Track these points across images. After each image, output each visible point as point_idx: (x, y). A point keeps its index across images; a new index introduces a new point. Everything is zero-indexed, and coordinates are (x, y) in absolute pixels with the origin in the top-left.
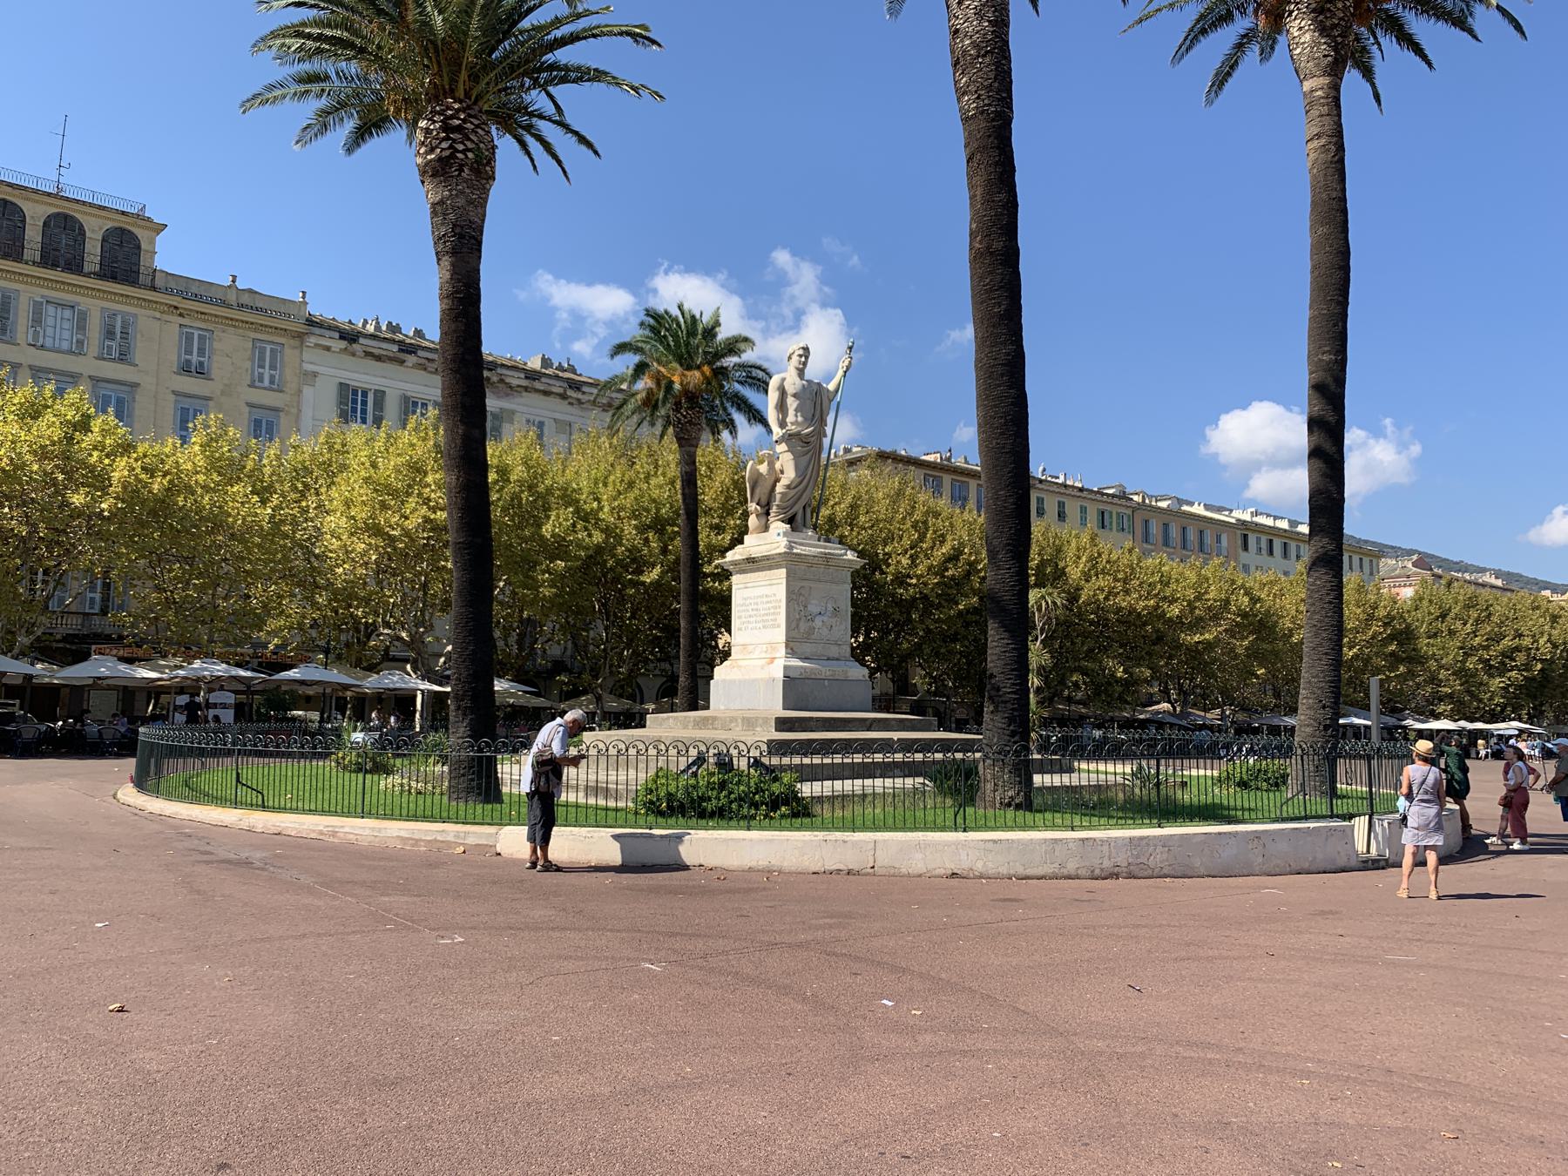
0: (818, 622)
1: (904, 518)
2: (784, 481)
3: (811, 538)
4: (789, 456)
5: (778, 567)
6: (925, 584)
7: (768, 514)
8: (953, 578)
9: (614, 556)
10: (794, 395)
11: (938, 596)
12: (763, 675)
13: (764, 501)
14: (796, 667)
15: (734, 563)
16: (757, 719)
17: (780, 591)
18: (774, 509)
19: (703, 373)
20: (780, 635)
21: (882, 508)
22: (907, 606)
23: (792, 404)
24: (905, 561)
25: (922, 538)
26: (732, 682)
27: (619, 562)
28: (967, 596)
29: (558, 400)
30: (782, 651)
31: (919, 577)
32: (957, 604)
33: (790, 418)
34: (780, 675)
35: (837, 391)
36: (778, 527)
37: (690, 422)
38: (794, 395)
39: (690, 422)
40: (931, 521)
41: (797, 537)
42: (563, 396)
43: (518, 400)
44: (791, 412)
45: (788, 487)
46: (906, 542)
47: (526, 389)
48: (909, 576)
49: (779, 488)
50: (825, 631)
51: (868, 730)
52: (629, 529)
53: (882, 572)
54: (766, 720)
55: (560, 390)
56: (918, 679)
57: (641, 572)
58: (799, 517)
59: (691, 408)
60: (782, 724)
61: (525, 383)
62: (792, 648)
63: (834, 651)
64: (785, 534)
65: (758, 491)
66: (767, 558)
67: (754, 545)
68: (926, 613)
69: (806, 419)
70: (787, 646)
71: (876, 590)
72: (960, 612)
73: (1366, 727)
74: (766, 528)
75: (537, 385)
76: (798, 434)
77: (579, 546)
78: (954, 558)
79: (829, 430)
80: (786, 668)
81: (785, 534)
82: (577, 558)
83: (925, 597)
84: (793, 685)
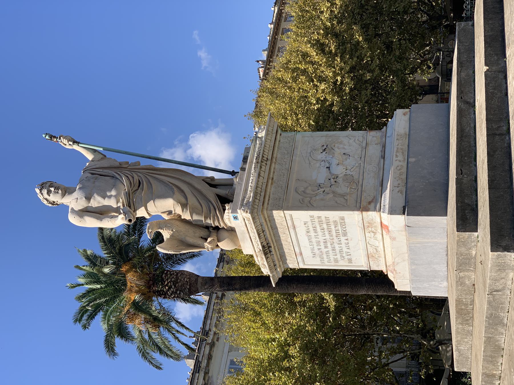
0: (339, 170)
1: (290, 88)
2: (178, 210)
3: (241, 179)
4: (151, 205)
5: (272, 220)
6: (341, 69)
7: (217, 229)
8: (337, 48)
9: (314, 333)
10: (88, 198)
11: (351, 58)
12: (402, 238)
13: (203, 233)
14: (392, 198)
15: (273, 267)
16: (459, 254)
17: (301, 217)
18: (210, 222)
19: (128, 271)
20: (353, 218)
21: (281, 106)
22: (359, 82)
23: (97, 201)
24: (323, 86)
25: (304, 72)
26: (413, 272)
27: (320, 328)
28: (352, 35)
29: (215, 349)
30: (372, 215)
31: (335, 74)
32: (358, 42)
33: (112, 203)
34: (401, 220)
35: (95, 151)
36: (229, 218)
37: (175, 283)
38: (88, 198)
39: (175, 283)
40: (291, 66)
41: (238, 197)
42: (212, 345)
43: (214, 379)
44: (106, 202)
45: (184, 206)
46: (307, 85)
47: (206, 373)
48: (335, 83)
49: (187, 216)
50: (350, 162)
51: (473, 105)
52: (293, 320)
53: (332, 105)
54: (460, 243)
55: (208, 348)
56: (424, 77)
57: (327, 309)
58: (222, 192)
59: (163, 281)
60: (467, 221)
61: (202, 374)
62: (366, 203)
63: (374, 151)
64: (234, 211)
65: (191, 240)
66: (261, 233)
67: (250, 245)
68: (367, 67)
69: (114, 186)
70: (366, 209)
71: (347, 109)
72: (365, 40)
73: (440, 315)
74: (232, 230)
75: (204, 364)
76: (128, 195)
77: (301, 367)
78: (321, 47)
79: (132, 160)
80: (392, 212)
81: (234, 211)
82: (313, 370)
83: (352, 69)
84: (412, 205)
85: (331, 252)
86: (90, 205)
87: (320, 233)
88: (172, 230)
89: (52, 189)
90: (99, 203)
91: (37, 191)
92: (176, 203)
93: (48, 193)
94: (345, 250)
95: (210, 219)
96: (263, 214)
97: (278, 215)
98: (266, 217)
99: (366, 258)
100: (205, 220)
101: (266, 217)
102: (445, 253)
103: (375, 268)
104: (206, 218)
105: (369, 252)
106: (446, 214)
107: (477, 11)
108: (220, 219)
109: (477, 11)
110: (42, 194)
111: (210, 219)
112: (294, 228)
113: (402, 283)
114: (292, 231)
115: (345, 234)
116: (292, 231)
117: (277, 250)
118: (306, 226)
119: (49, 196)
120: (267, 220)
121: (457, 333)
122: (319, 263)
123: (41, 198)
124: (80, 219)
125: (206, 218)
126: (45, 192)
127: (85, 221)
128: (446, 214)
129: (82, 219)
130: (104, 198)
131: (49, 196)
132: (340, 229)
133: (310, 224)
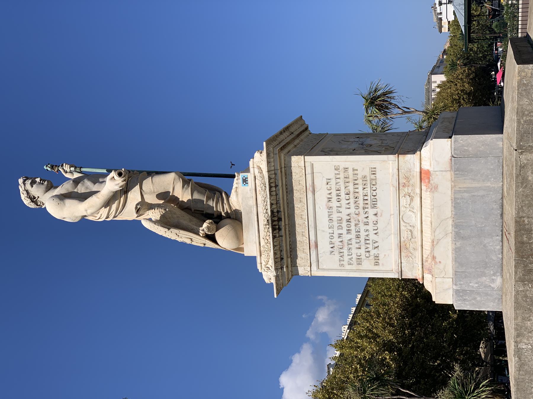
74: (235, 218)
85: (354, 241)
86: (76, 190)
87: (344, 202)
88: (165, 210)
89: (38, 180)
90: (87, 188)
91: (21, 181)
92: (177, 177)
93: (31, 183)
94: (372, 237)
95: (213, 200)
96: (280, 157)
97: (297, 161)
98: (283, 166)
99: (398, 251)
100: (207, 201)
101: (283, 166)
102: (499, 212)
103: (408, 275)
104: (208, 198)
105: (402, 239)
106: (500, 130)
107: (506, 91)
108: (225, 201)
109: (506, 91)
110: (24, 184)
111: (213, 200)
112: (314, 192)
113: (442, 293)
114: (310, 195)
115: (374, 206)
116: (310, 195)
117: (287, 232)
118: (328, 186)
119: (32, 187)
120: (283, 170)
121: (517, 384)
122: (336, 266)
123: (21, 189)
124: (59, 202)
125: (208, 198)
126: (28, 182)
127: (64, 204)
128: (500, 130)
129: (62, 202)
130: (95, 183)
131: (32, 187)
132: (369, 194)
133: (333, 182)
